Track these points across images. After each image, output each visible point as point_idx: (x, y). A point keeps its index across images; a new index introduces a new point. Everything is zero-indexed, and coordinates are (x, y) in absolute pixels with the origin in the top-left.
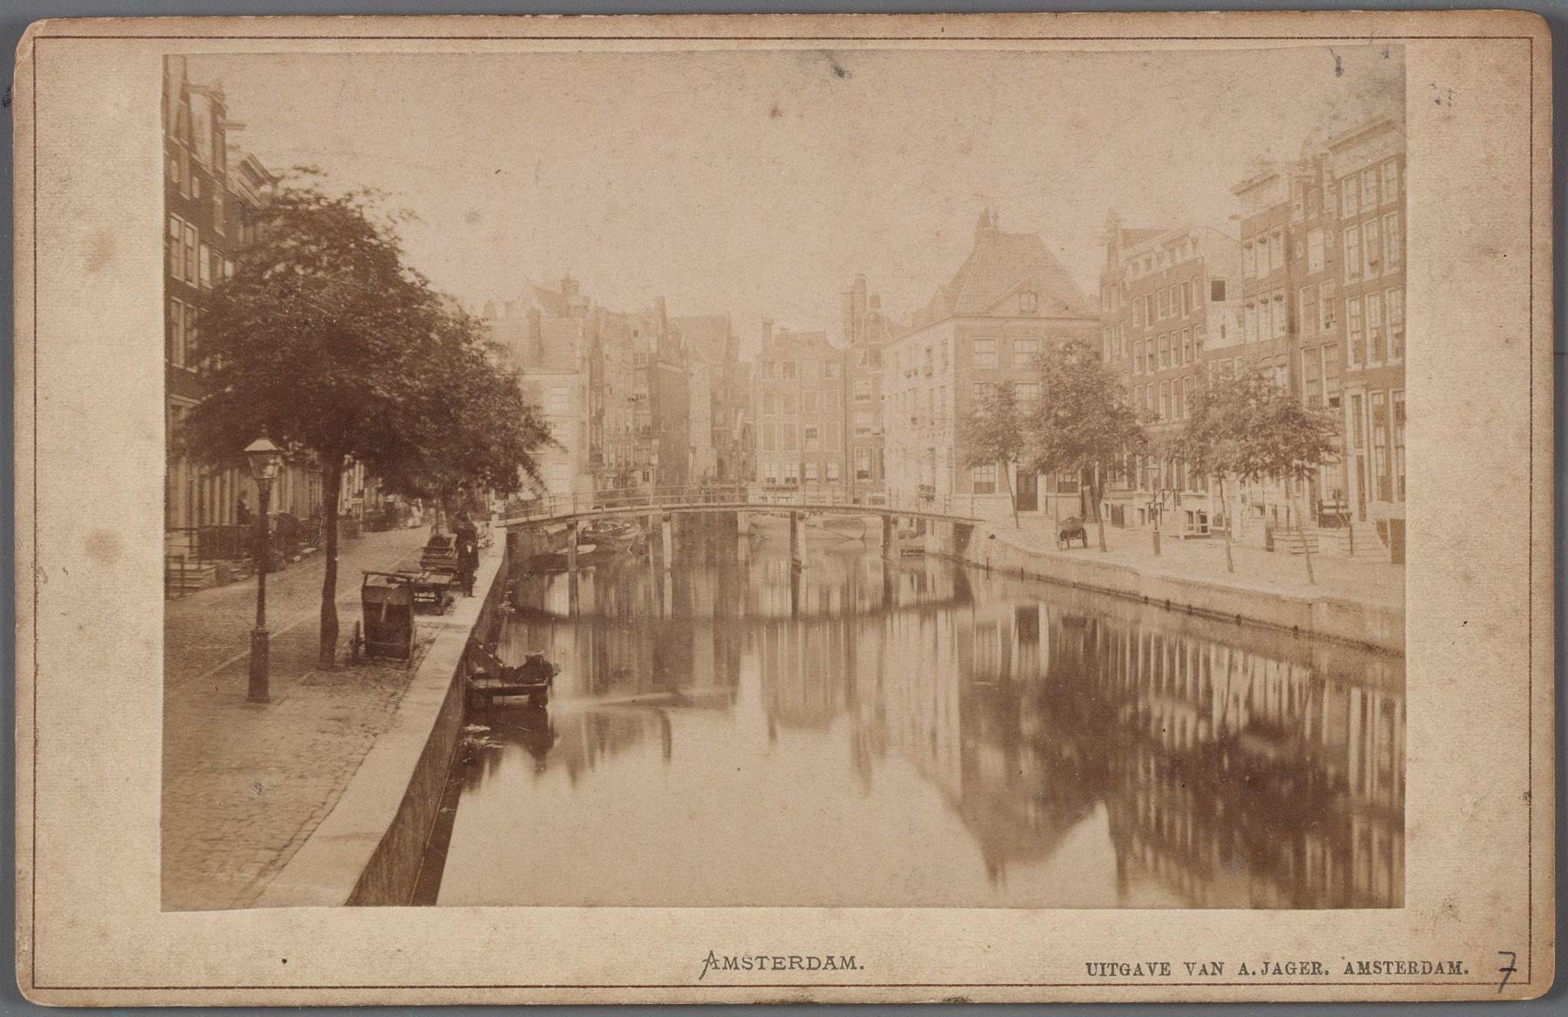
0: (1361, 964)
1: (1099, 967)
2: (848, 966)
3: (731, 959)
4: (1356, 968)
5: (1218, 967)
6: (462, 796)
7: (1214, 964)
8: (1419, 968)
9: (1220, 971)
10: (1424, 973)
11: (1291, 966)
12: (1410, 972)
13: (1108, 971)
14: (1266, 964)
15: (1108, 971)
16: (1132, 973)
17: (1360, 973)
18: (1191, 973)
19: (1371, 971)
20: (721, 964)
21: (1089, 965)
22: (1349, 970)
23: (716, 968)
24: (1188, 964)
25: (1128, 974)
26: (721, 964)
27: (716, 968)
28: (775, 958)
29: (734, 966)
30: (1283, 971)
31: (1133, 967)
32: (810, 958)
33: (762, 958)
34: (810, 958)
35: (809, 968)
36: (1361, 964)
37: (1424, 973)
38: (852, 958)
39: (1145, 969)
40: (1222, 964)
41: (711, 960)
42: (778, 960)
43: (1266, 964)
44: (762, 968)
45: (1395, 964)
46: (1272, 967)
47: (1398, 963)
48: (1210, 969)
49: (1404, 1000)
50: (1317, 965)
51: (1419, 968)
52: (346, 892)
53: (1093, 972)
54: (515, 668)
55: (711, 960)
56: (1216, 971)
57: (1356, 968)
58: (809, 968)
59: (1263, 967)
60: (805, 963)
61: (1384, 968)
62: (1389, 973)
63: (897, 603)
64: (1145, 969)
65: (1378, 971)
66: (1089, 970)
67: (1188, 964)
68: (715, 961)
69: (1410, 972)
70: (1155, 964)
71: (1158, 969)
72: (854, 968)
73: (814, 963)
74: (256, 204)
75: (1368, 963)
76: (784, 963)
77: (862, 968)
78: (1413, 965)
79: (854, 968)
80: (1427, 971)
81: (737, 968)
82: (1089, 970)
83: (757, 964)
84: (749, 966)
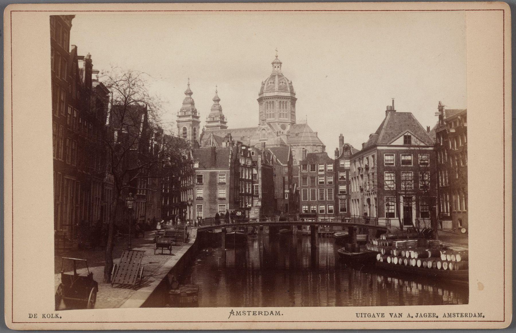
0: (448, 314)
1: (360, 314)
2: (238, 314)
3: (278, 312)
4: (447, 315)
5: (35, 316)
6: (333, 251)
7: (399, 314)
8: (468, 315)
9: (401, 316)
10: (470, 317)
11: (425, 314)
12: (433, 317)
13: (363, 316)
14: (417, 314)
15: (363, 316)
16: (371, 316)
17: (478, 317)
18: (378, 316)
19: (452, 316)
20: (235, 313)
21: (357, 314)
22: (445, 316)
23: (234, 315)
24: (377, 314)
25: (426, 317)
26: (235, 313)
27: (234, 315)
28: (253, 312)
29: (239, 314)
30: (423, 316)
31: (372, 315)
32: (265, 312)
33: (249, 312)
34: (265, 312)
35: (265, 315)
36: (448, 314)
37: (470, 317)
38: (279, 312)
39: (376, 315)
40: (402, 314)
41: (232, 312)
42: (254, 312)
43: (417, 314)
44: (249, 315)
45: (460, 314)
46: (419, 315)
47: (461, 314)
48: (398, 315)
49: (423, 329)
50: (434, 314)
51: (468, 315)
52: (142, 301)
53: (358, 316)
54: (61, 283)
55: (232, 312)
56: (400, 316)
57: (447, 315)
58: (265, 315)
59: (416, 315)
60: (263, 313)
61: (456, 315)
62: (458, 317)
63: (349, 167)
64: (376, 315)
65: (454, 316)
66: (357, 315)
67: (377, 314)
68: (233, 312)
69: (433, 317)
70: (379, 313)
71: (380, 315)
72: (280, 315)
73: (267, 313)
74: (148, 121)
75: (451, 314)
76: (256, 313)
77: (282, 315)
78: (466, 314)
79: (280, 315)
80: (471, 316)
81: (240, 315)
82: (357, 315)
83: (456, 315)
84: (245, 314)
